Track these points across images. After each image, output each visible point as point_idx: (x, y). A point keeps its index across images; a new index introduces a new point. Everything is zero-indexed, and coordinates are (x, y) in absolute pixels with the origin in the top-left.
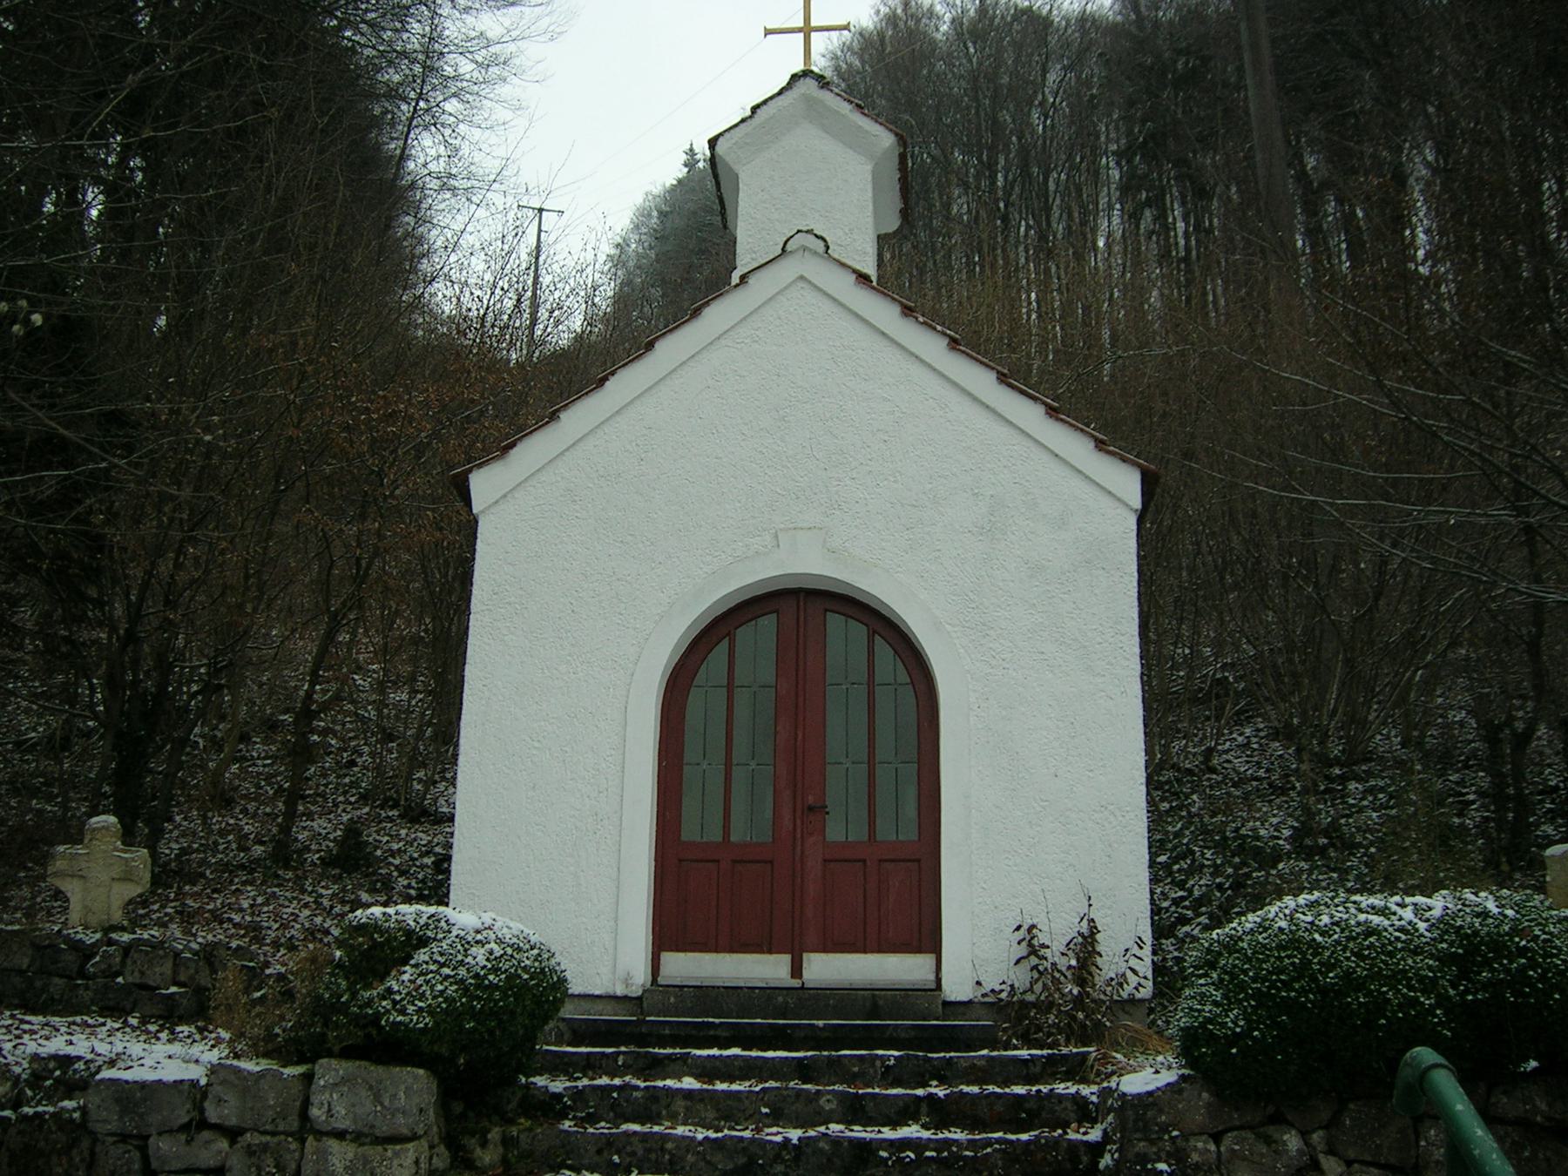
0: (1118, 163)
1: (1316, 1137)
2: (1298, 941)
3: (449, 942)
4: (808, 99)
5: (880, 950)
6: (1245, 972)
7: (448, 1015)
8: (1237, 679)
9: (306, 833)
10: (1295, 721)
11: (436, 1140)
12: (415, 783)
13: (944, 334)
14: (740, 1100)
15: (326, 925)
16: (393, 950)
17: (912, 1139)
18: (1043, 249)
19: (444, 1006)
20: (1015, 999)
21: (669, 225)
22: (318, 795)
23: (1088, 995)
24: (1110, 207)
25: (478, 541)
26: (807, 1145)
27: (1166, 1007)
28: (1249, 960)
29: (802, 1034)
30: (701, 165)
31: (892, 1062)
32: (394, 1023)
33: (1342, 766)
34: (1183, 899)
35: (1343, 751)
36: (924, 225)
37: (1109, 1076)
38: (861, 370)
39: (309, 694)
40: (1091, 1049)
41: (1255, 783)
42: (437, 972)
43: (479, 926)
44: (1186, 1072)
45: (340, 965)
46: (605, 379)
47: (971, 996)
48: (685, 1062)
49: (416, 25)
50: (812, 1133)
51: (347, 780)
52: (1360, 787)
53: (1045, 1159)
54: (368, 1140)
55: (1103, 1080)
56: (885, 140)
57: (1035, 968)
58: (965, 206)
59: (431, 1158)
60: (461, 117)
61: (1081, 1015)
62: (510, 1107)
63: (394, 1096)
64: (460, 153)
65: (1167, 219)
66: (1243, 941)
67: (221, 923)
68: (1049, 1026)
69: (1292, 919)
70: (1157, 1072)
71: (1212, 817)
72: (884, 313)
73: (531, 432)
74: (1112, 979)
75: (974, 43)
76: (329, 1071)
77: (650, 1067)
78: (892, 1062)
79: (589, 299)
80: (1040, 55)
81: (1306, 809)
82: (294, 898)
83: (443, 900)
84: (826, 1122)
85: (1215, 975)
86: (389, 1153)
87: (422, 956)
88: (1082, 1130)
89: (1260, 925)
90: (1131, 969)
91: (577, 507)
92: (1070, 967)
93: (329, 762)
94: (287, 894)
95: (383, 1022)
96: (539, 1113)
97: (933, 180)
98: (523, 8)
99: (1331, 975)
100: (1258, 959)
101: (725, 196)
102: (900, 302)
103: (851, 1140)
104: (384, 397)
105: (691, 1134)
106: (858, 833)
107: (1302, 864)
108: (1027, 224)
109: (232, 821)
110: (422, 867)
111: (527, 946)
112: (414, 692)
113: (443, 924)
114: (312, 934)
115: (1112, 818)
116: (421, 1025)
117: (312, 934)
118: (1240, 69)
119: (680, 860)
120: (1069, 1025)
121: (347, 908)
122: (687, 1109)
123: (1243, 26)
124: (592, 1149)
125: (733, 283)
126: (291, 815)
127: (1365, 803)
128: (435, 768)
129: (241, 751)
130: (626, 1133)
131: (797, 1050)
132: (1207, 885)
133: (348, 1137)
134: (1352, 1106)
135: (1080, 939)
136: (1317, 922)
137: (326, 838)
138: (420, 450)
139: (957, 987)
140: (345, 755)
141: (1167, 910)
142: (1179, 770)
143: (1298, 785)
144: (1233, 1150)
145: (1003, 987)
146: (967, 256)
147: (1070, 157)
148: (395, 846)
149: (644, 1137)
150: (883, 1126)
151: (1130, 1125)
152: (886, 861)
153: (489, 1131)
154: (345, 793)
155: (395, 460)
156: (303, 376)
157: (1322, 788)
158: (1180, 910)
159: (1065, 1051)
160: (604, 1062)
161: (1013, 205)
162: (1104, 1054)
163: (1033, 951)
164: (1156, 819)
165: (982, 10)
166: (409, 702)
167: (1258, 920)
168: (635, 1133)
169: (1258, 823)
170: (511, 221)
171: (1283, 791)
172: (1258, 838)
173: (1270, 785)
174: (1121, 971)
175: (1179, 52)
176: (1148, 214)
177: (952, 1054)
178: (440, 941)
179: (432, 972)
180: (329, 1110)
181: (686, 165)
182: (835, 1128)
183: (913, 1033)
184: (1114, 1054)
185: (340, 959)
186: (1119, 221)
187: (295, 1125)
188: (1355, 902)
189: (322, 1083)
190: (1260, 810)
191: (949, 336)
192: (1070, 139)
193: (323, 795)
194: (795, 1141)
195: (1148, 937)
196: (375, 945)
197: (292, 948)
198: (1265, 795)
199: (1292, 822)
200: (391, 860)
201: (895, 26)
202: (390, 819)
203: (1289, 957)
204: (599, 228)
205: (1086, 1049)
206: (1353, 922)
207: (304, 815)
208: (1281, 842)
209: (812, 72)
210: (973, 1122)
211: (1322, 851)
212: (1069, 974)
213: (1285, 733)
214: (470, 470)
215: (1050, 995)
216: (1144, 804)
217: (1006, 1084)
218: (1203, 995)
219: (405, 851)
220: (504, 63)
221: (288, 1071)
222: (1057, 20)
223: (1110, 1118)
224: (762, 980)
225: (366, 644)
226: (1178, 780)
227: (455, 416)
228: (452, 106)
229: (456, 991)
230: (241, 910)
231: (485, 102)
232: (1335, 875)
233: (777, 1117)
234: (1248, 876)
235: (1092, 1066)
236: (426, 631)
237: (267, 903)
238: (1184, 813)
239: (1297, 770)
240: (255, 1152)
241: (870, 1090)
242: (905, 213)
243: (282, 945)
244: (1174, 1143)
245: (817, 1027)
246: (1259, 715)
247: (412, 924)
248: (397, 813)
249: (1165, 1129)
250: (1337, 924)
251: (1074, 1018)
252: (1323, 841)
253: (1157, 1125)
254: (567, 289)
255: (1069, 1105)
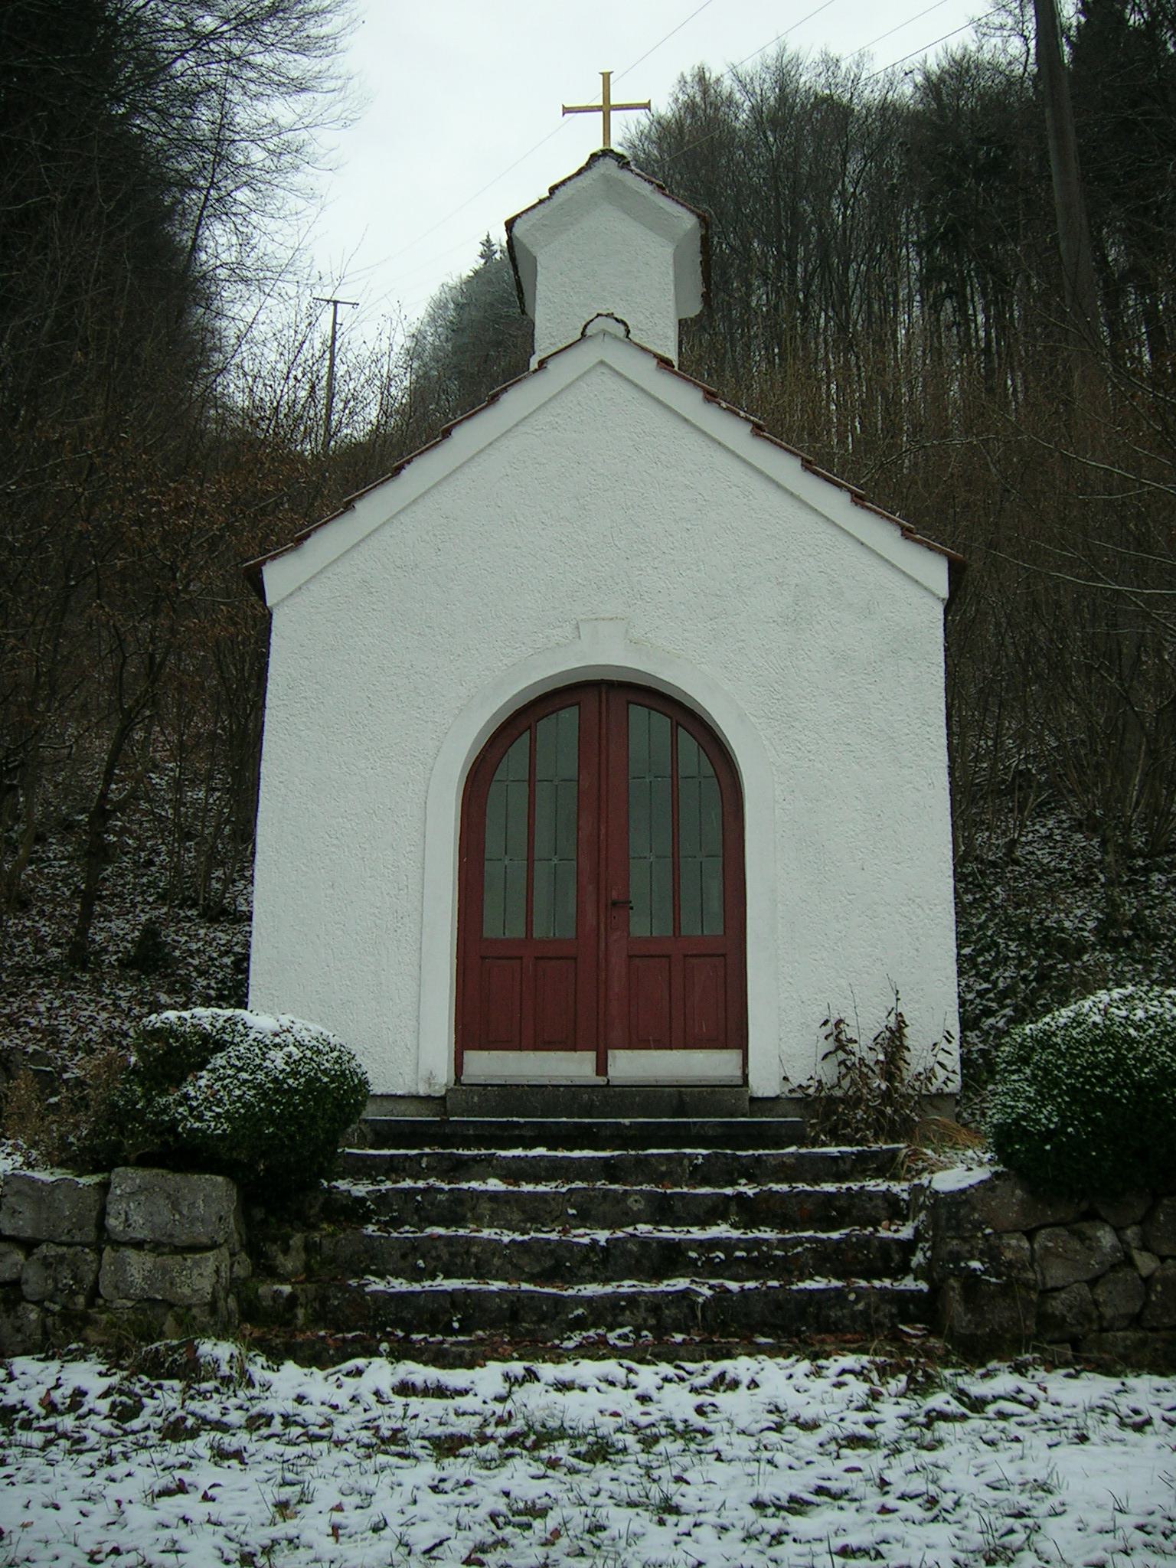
0: (919, 254)
1: (1130, 1233)
2: (1113, 1036)
3: (246, 1045)
4: (606, 179)
5: (686, 1046)
6: (1059, 1068)
7: (247, 1121)
8: (1041, 771)
9: (104, 934)
10: (1098, 813)
11: (237, 1248)
12: (214, 882)
13: (747, 419)
14: (546, 1201)
15: (125, 1028)
16: (189, 1055)
17: (721, 1239)
18: (845, 340)
19: (242, 1111)
20: (823, 1094)
21: (466, 316)
22: (116, 895)
23: (896, 1089)
24: (910, 299)
25: (273, 635)
26: (615, 1246)
27: (971, 1100)
28: (1062, 1055)
29: (608, 1133)
30: (498, 256)
31: (700, 1161)
32: (192, 1130)
33: (1145, 857)
34: (987, 991)
35: (1146, 843)
36: (723, 317)
37: (919, 1172)
38: (663, 457)
39: (103, 795)
40: (902, 1145)
41: (1057, 875)
42: (235, 1077)
43: (277, 1028)
44: (1000, 1168)
45: (135, 1071)
46: (401, 468)
47: (778, 1092)
48: (490, 1163)
49: (204, 110)
50: (619, 1234)
51: (145, 880)
52: (1164, 879)
53: (855, 1257)
54: (166, 1250)
55: (913, 1177)
56: (687, 221)
57: (842, 1063)
58: (764, 297)
59: (232, 1266)
60: (253, 207)
61: (889, 1110)
62: (312, 1212)
63: (192, 1205)
64: (252, 242)
65: (967, 311)
66: (1056, 1036)
67: (18, 1027)
68: (858, 1121)
69: (1106, 1013)
70: (970, 1169)
71: (1016, 909)
72: (686, 398)
73: (325, 523)
74: (920, 1074)
75: (774, 132)
76: (126, 1179)
77: (454, 1169)
78: (700, 1161)
79: (385, 389)
80: (840, 145)
81: (1111, 901)
82: (92, 1001)
83: (243, 1004)
84: (633, 1223)
85: (1028, 1071)
86: (189, 1263)
87: (219, 1060)
88: (893, 1228)
89: (1074, 1020)
90: (939, 1063)
91: (374, 599)
92: (877, 1062)
93: (126, 862)
94: (85, 997)
95: (180, 1129)
96: (342, 1218)
97: (732, 271)
98: (316, 95)
99: (1146, 1070)
100: (1071, 1054)
101: (522, 279)
102: (702, 387)
103: (659, 1240)
104: (176, 489)
105: (497, 1237)
106: (662, 928)
107: (1107, 955)
108: (826, 314)
109: (28, 923)
110: (222, 967)
111: (327, 1049)
112: (211, 790)
113: (240, 1027)
114: (111, 1037)
115: (919, 911)
116: (219, 1132)
117: (111, 1037)
118: (1043, 159)
119: (483, 958)
120: (877, 1119)
121: (146, 1010)
122: (493, 1211)
123: (1048, 112)
124: (397, 1254)
125: (532, 368)
126: (87, 916)
127: (1169, 894)
128: (233, 866)
129: (36, 852)
130: (431, 1237)
131: (603, 1149)
132: (1012, 977)
133: (147, 1247)
134: (1165, 1202)
135: (888, 1034)
136: (1131, 1017)
137: (123, 939)
138: (213, 543)
139: (764, 1083)
140: (143, 854)
141: (972, 1002)
142: (982, 862)
143: (1101, 876)
144: (1046, 1247)
145: (811, 1082)
146: (766, 349)
147: (870, 249)
148: (194, 947)
149: (449, 1241)
150: (692, 1225)
151: (943, 1223)
152: (691, 956)
153: (290, 1237)
154: (143, 893)
155: (187, 554)
156: (92, 470)
157: (1126, 879)
158: (984, 1002)
159: (875, 1147)
160: (407, 1165)
161: (812, 296)
162: (915, 1151)
163: (841, 1046)
164: (962, 911)
165: (782, 99)
166: (207, 801)
167: (1072, 1015)
168: (440, 1237)
169: (1062, 915)
170: (304, 310)
171: (1087, 883)
172: (1063, 930)
173: (1074, 876)
174: (928, 1066)
175: (981, 141)
176: (949, 306)
177: (761, 1152)
178: (237, 1044)
179: (229, 1076)
180: (127, 1220)
181: (482, 256)
182: (643, 1228)
183: (720, 1130)
184: (925, 1150)
185: (135, 1065)
186: (918, 312)
187: (90, 1234)
188: (1169, 996)
189: (118, 1192)
190: (1063, 902)
191: (753, 422)
192: (870, 229)
193: (120, 896)
194: (603, 1243)
195: (956, 1031)
196: (171, 1050)
197: (89, 1051)
198: (1067, 887)
199: (1095, 913)
200: (190, 960)
201: (694, 115)
202: (189, 919)
203: (1103, 1052)
204: (395, 317)
205: (896, 1145)
206: (1168, 1017)
207: (101, 915)
208: (1086, 934)
209: (612, 151)
210: (782, 1222)
211: (1127, 943)
212: (876, 1069)
213: (1088, 825)
214: (263, 562)
215: (859, 1090)
216: (952, 897)
217: (816, 1181)
218: (1016, 1091)
219: (204, 952)
220: (297, 151)
221: (83, 1180)
222: (858, 108)
223: (922, 1216)
224: (567, 1077)
225: (163, 743)
226: (981, 872)
227: (248, 508)
228: (243, 195)
229: (254, 1096)
230: (38, 1014)
231: (277, 191)
232: (1140, 967)
233: (585, 1218)
234: (1053, 967)
235: (903, 1163)
236: (223, 728)
237: (64, 1006)
238: (987, 905)
239: (1101, 862)
240: (51, 1264)
241: (678, 1190)
242: (706, 298)
243: (80, 1048)
244: (987, 1241)
245: (624, 1125)
246: (1063, 807)
247: (208, 1027)
248: (196, 913)
249: (978, 1226)
250: (1152, 1018)
251: (883, 1113)
252: (1127, 932)
253: (970, 1222)
254: (363, 379)
255: (879, 1202)
